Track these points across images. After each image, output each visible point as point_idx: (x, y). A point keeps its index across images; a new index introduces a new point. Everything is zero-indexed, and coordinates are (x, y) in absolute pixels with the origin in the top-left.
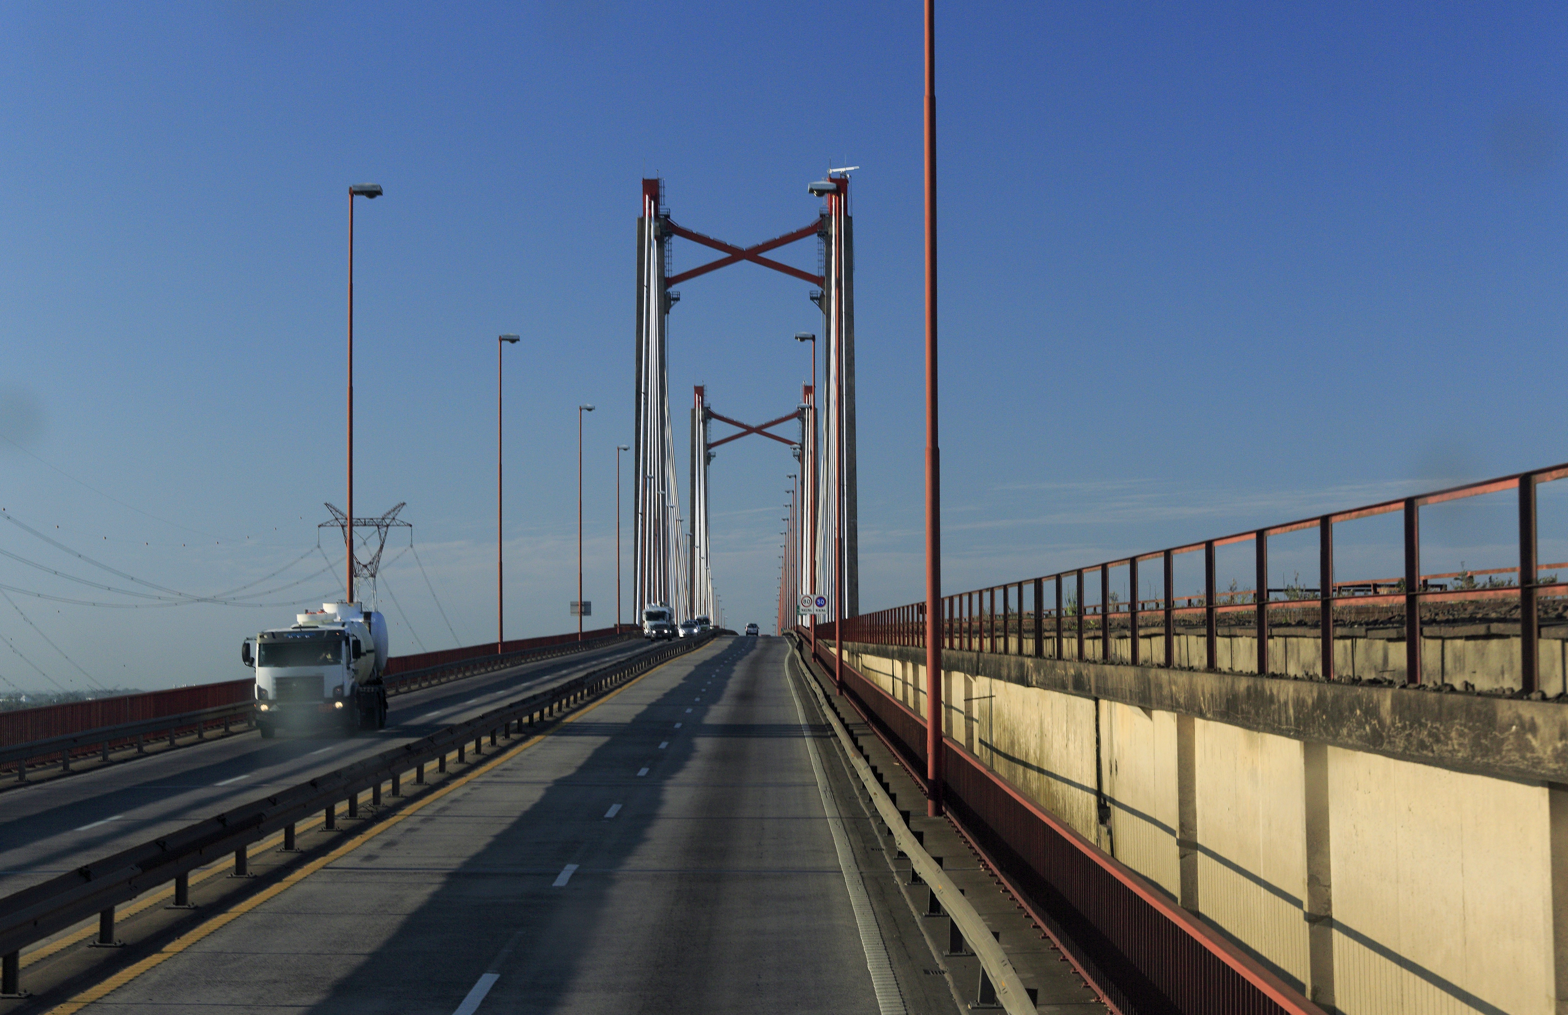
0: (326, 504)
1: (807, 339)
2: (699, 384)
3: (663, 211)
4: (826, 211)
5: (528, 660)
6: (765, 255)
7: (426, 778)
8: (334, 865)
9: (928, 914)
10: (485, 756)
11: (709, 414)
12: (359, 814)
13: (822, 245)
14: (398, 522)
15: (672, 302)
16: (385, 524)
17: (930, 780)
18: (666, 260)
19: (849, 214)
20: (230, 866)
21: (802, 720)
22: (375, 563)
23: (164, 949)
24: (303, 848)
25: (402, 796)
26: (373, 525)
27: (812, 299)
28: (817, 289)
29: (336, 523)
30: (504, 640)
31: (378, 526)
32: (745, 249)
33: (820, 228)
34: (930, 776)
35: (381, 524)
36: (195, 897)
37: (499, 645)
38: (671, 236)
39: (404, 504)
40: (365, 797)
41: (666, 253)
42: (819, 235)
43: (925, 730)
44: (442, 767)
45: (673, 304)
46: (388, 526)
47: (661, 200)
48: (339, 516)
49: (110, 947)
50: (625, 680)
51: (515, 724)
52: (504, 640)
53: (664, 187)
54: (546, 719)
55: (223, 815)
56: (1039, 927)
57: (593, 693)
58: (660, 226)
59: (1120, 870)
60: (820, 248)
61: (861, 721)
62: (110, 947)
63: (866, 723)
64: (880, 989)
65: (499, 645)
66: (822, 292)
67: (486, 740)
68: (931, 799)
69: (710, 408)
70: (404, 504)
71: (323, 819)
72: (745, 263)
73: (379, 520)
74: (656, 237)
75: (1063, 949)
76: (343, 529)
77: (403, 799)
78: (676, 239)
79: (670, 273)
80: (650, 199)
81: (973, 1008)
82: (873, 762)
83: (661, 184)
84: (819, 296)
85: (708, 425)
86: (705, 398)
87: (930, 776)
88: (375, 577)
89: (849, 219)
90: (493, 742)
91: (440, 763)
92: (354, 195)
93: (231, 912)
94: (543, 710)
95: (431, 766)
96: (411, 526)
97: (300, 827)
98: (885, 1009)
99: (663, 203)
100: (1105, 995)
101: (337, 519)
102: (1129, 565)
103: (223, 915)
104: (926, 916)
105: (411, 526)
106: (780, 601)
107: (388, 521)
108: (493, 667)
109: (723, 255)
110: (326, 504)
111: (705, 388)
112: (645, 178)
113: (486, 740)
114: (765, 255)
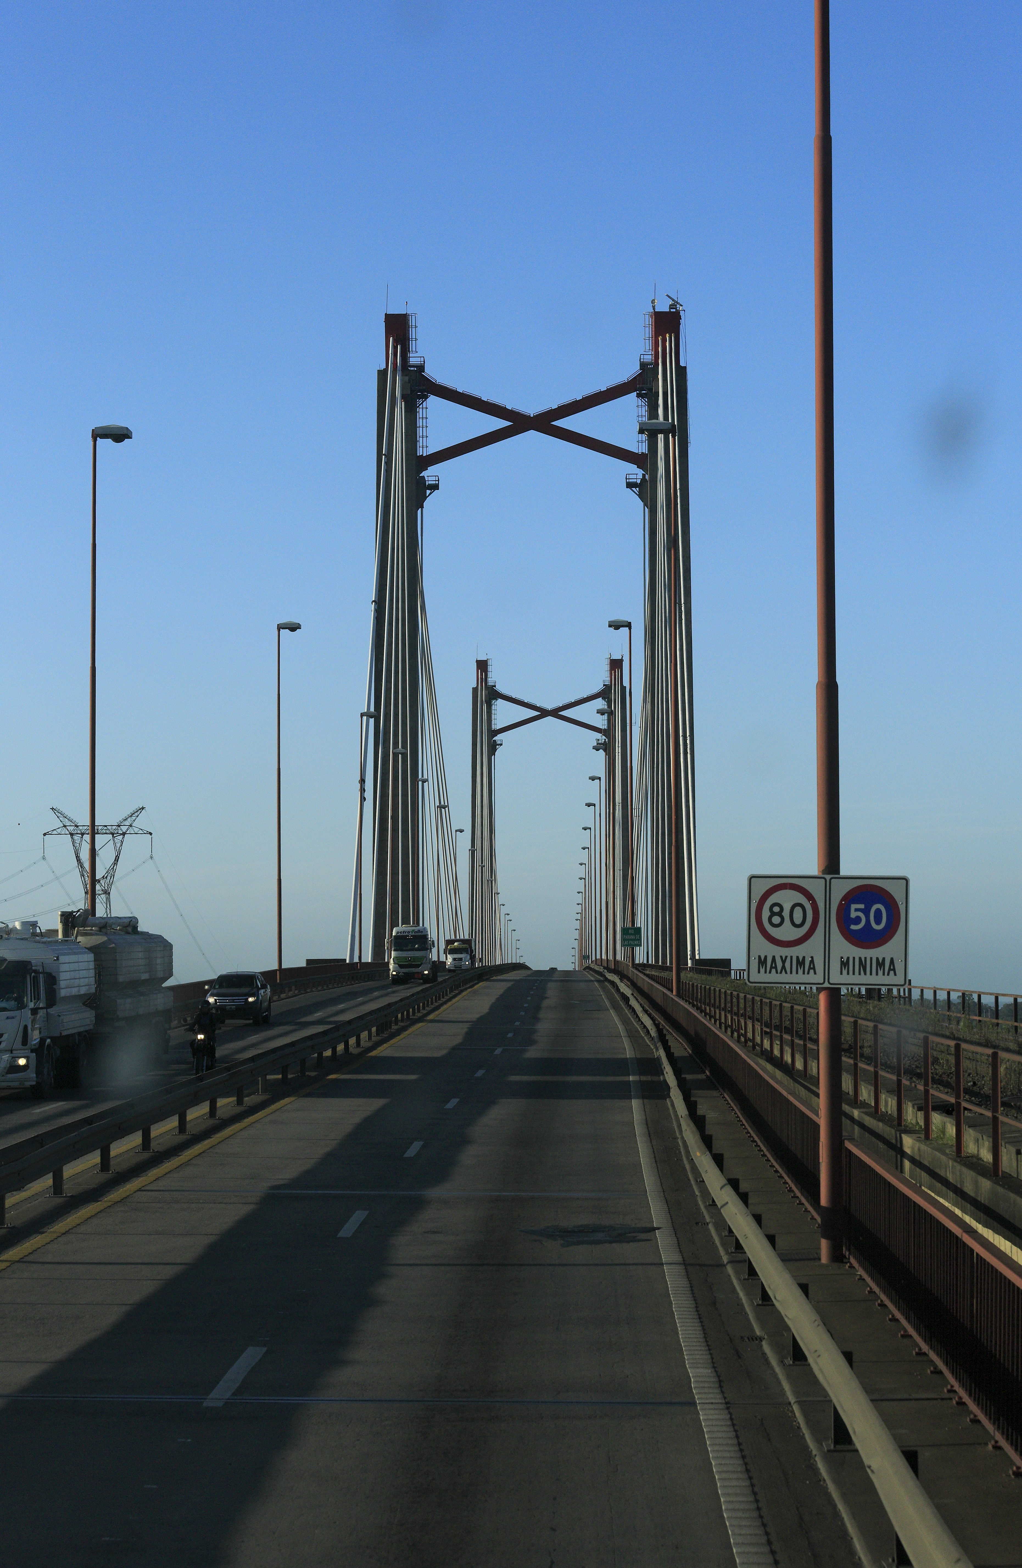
0: (52, 809)
1: (623, 626)
2: (482, 658)
3: (413, 360)
4: (649, 358)
6: (562, 423)
9: (832, 1447)
11: (493, 694)
13: (644, 408)
14: (136, 830)
15: (428, 492)
16: (120, 832)
17: (824, 1207)
18: (420, 432)
19: (682, 364)
20: (206, 1112)
22: (109, 878)
24: (161, 1148)
25: (373, 1041)
26: (106, 833)
27: (630, 485)
28: (636, 473)
29: (65, 831)
30: (284, 966)
31: (113, 834)
32: (532, 416)
33: (605, 693)
34: (824, 1201)
35: (118, 832)
36: (219, 1113)
38: (426, 397)
39: (143, 808)
41: (420, 423)
42: (638, 396)
43: (817, 1127)
46: (124, 834)
47: (412, 345)
48: (68, 823)
51: (314, 1058)
52: (284, 966)
53: (416, 327)
54: (351, 1049)
56: (897, 1320)
57: (428, 1006)
58: (409, 382)
59: (938, 1209)
60: (640, 414)
64: (674, 1290)
65: (278, 972)
66: (644, 475)
69: (495, 686)
70: (143, 808)
71: (50, 1182)
72: (532, 436)
73: (114, 827)
74: (404, 397)
75: (933, 1356)
76: (72, 838)
77: (363, 1049)
78: (433, 402)
79: (425, 449)
80: (396, 343)
82: (718, 1147)
83: (412, 322)
84: (639, 481)
85: (493, 707)
86: (489, 675)
87: (824, 1201)
88: (109, 894)
89: (682, 372)
92: (98, 438)
94: (397, 1016)
96: (151, 834)
97: (156, 1131)
98: (730, 1506)
99: (414, 349)
100: (881, 1292)
101: (65, 826)
104: (758, 1305)
105: (151, 834)
106: (581, 920)
107: (124, 829)
109: (502, 424)
110: (52, 809)
111: (489, 663)
112: (392, 311)
114: (562, 423)
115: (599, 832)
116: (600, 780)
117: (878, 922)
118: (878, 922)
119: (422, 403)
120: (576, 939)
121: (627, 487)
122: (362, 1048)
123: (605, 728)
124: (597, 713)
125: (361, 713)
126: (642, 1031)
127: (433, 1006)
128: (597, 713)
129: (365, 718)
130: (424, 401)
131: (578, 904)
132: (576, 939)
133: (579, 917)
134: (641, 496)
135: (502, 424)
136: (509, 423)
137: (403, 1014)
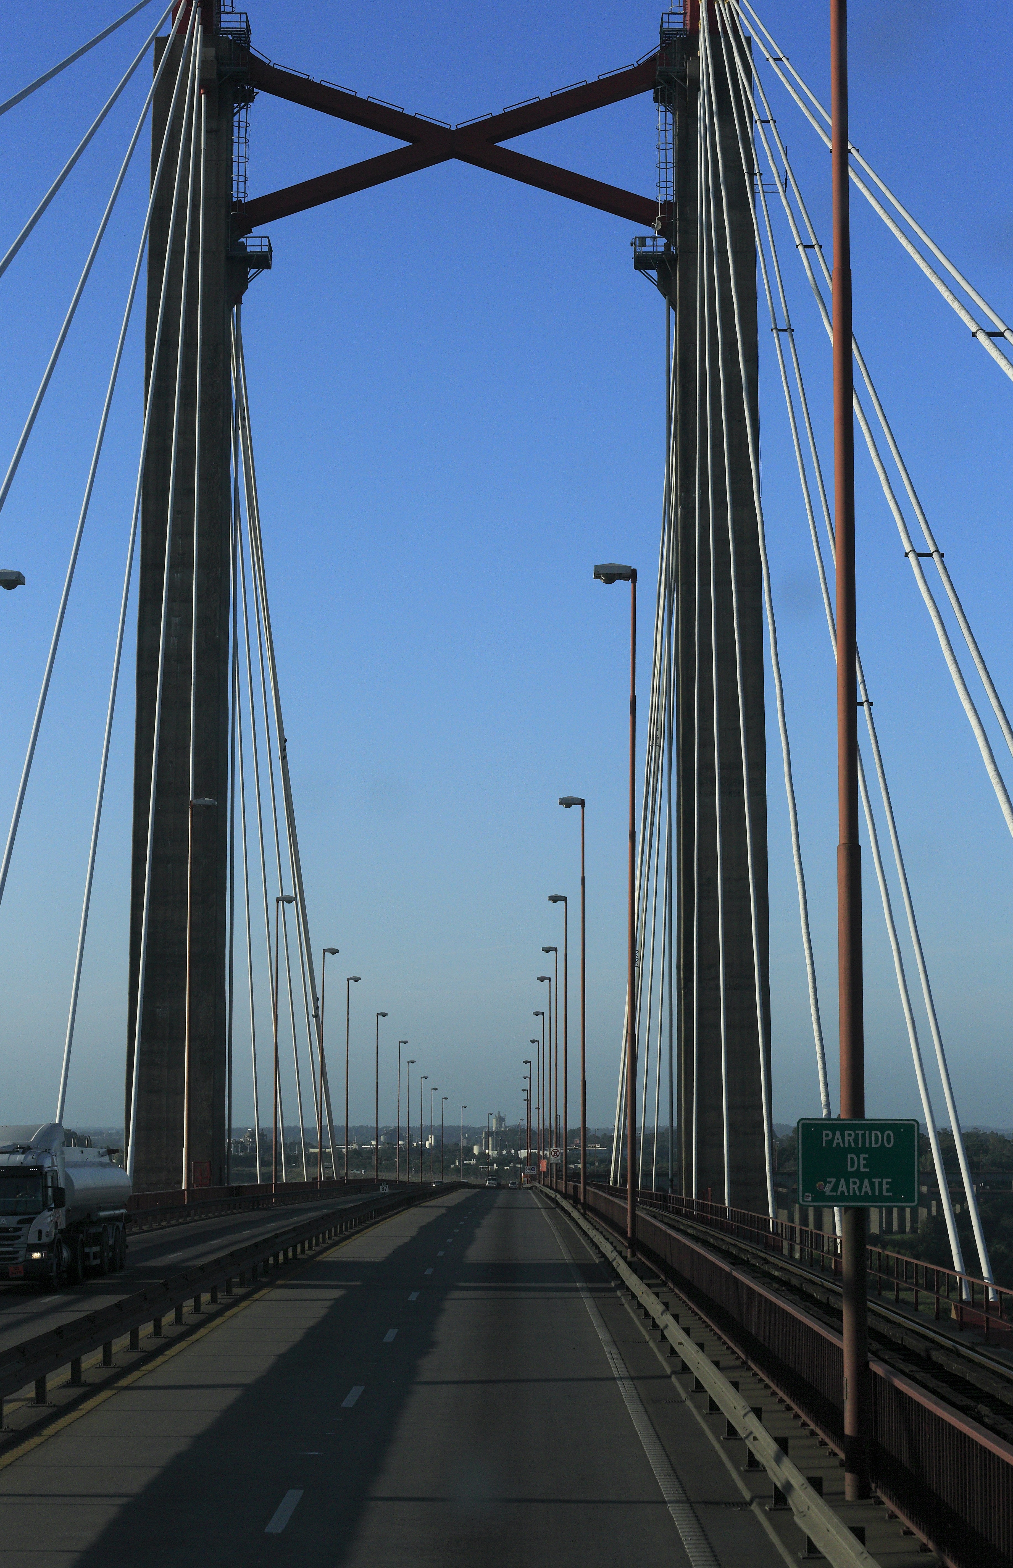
4: (677, 23)
5: (145, 1228)
7: (141, 1344)
8: (141, 1383)
10: (188, 1327)
12: (219, 1301)
21: (619, 1382)
23: (140, 1369)
25: (235, 1295)
37: (186, 1192)
38: (249, 98)
40: (120, 1343)
44: (134, 1344)
45: (255, 275)
49: (111, 1368)
50: (324, 1245)
55: (59, 1327)
61: (739, 1363)
62: (111, 1368)
63: (744, 1363)
65: (186, 1192)
67: (206, 1297)
68: (850, 1472)
81: (771, 1509)
90: (214, 1300)
91: (154, 1327)
93: (81, 1410)
95: (91, 1360)
102: (232, 1127)
103: (137, 1372)
104: (746, 1471)
108: (178, 1220)
109: (390, 144)
113: (146, 1330)
115: (555, 1005)
116: (543, 1016)
117: (889, 1142)
118: (889, 1142)
119: (238, 112)
120: (524, 1090)
121: (636, 268)
122: (220, 1304)
123: (670, 198)
124: (543, 950)
125: (277, 898)
126: (707, 1421)
127: (330, 1242)
128: (543, 950)
129: (281, 902)
130: (243, 107)
131: (525, 1078)
132: (524, 1090)
133: (546, 965)
134: (665, 286)
135: (390, 144)
136: (404, 144)
137: (295, 1251)
